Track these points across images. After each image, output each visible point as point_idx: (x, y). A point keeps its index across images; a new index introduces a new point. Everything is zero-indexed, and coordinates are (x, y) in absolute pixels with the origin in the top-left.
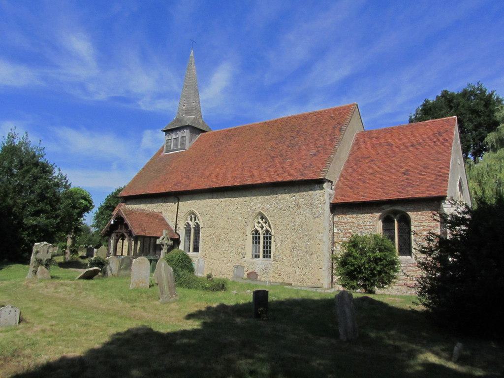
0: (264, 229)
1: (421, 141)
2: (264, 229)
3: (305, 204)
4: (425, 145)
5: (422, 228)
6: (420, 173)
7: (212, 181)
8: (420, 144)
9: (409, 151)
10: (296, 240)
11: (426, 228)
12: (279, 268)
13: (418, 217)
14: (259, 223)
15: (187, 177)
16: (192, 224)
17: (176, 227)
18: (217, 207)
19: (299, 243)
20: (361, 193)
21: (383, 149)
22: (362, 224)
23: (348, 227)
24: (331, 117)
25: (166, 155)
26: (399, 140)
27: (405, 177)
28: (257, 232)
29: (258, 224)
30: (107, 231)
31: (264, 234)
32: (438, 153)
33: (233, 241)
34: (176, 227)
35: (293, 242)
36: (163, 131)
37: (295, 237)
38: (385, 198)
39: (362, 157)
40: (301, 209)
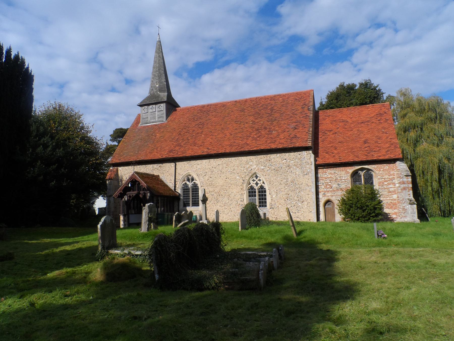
0: (259, 185)
1: (368, 119)
2: (259, 185)
3: (295, 165)
4: (373, 123)
5: (383, 180)
6: (376, 142)
7: (208, 148)
8: (368, 121)
9: (362, 127)
10: (289, 192)
11: (386, 179)
12: (276, 213)
13: (381, 172)
14: (254, 181)
15: (179, 145)
16: (190, 184)
17: (175, 187)
18: (215, 169)
19: (291, 194)
20: (337, 157)
21: (341, 124)
22: (339, 179)
23: (328, 181)
24: (296, 99)
25: (145, 127)
26: (351, 118)
27: (366, 145)
28: (252, 188)
29: (253, 182)
30: (120, 193)
31: (259, 189)
32: (384, 128)
33: (232, 196)
34: (175, 187)
35: (286, 194)
36: (403, 152)
37: (287, 190)
38: (357, 160)
39: (327, 130)
40: (292, 169)
